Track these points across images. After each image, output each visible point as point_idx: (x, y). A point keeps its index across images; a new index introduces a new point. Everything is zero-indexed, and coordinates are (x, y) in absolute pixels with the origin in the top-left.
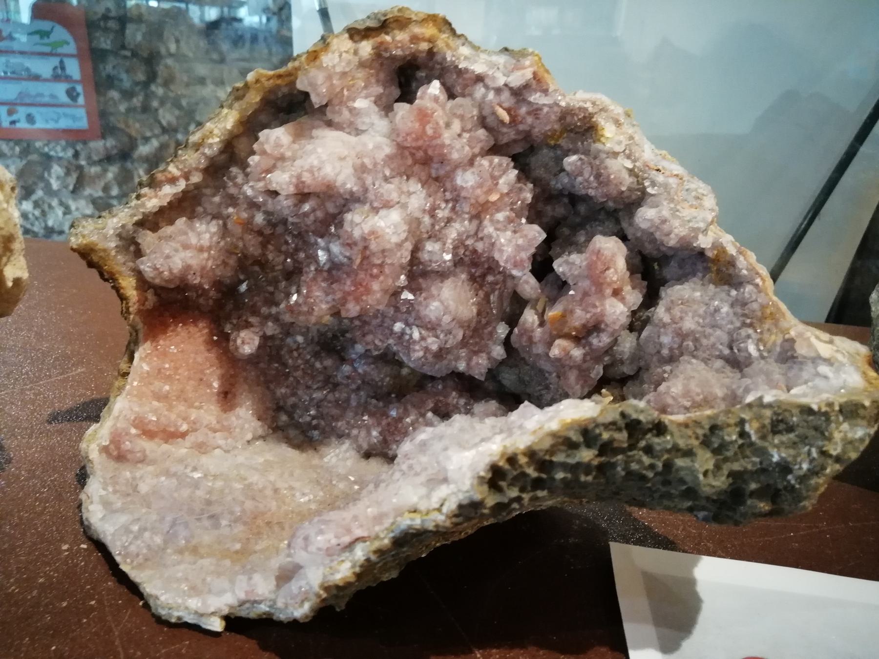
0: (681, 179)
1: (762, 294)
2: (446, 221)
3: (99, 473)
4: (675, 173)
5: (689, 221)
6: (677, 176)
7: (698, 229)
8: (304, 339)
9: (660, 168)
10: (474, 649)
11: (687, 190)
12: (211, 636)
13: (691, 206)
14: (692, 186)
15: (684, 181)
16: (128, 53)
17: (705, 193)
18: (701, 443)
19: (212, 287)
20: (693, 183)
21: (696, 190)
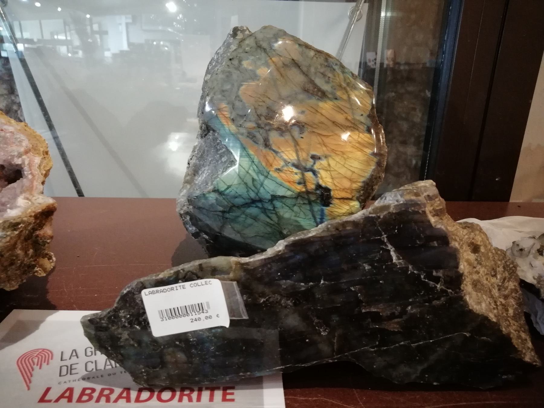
0: (13, 133)
1: (259, 112)
2: (313, 101)
3: (120, 294)
4: (10, 131)
5: (11, 152)
6: (11, 132)
7: (14, 155)
8: (290, 103)
9: (3, 129)
10: (395, 14)
11: (15, 138)
12: (343, 41)
13: (16, 145)
14: (18, 136)
15: (14, 134)
16: (342, 190)
17: (24, 139)
18: (218, 139)
19: (40, 216)
20: (18, 135)
21: (19, 138)
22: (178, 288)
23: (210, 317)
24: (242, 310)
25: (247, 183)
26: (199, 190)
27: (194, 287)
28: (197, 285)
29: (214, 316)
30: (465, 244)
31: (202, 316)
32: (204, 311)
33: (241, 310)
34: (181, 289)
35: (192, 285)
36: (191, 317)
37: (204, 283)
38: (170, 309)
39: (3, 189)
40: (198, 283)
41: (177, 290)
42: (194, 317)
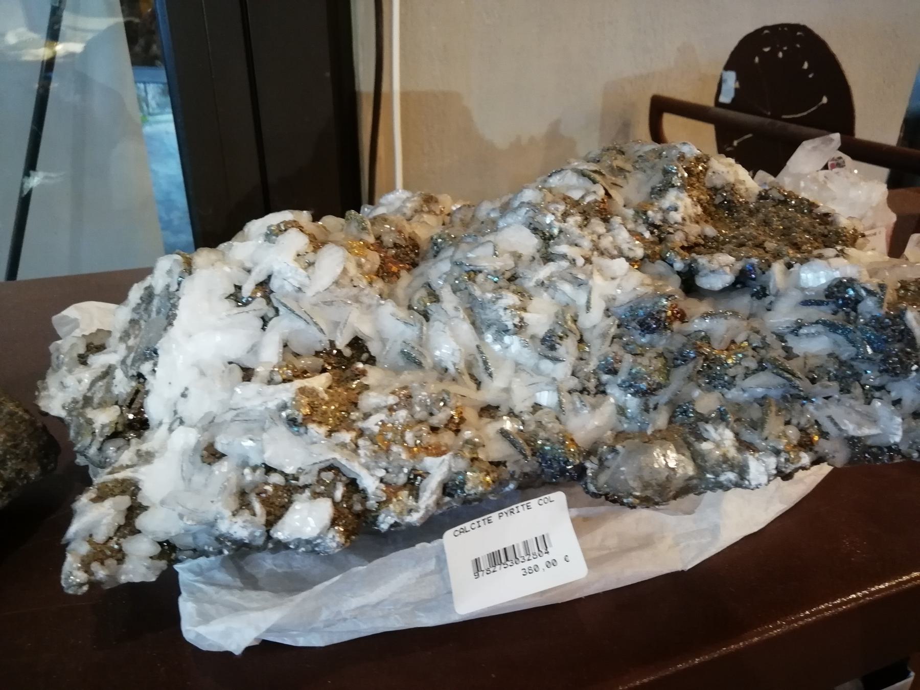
12: (382, 26)
22: (481, 523)
23: (554, 563)
24: (646, 542)
25: (575, 301)
26: (361, 442)
27: (544, 504)
28: (464, 531)
29: (560, 560)
30: (459, 256)
31: (541, 561)
32: (521, 559)
33: (286, 639)
34: (485, 524)
35: (457, 533)
36: (522, 565)
37: (477, 525)
38: (536, 538)
39: (893, 218)
40: (465, 527)
41: (519, 512)
42: (526, 565)
